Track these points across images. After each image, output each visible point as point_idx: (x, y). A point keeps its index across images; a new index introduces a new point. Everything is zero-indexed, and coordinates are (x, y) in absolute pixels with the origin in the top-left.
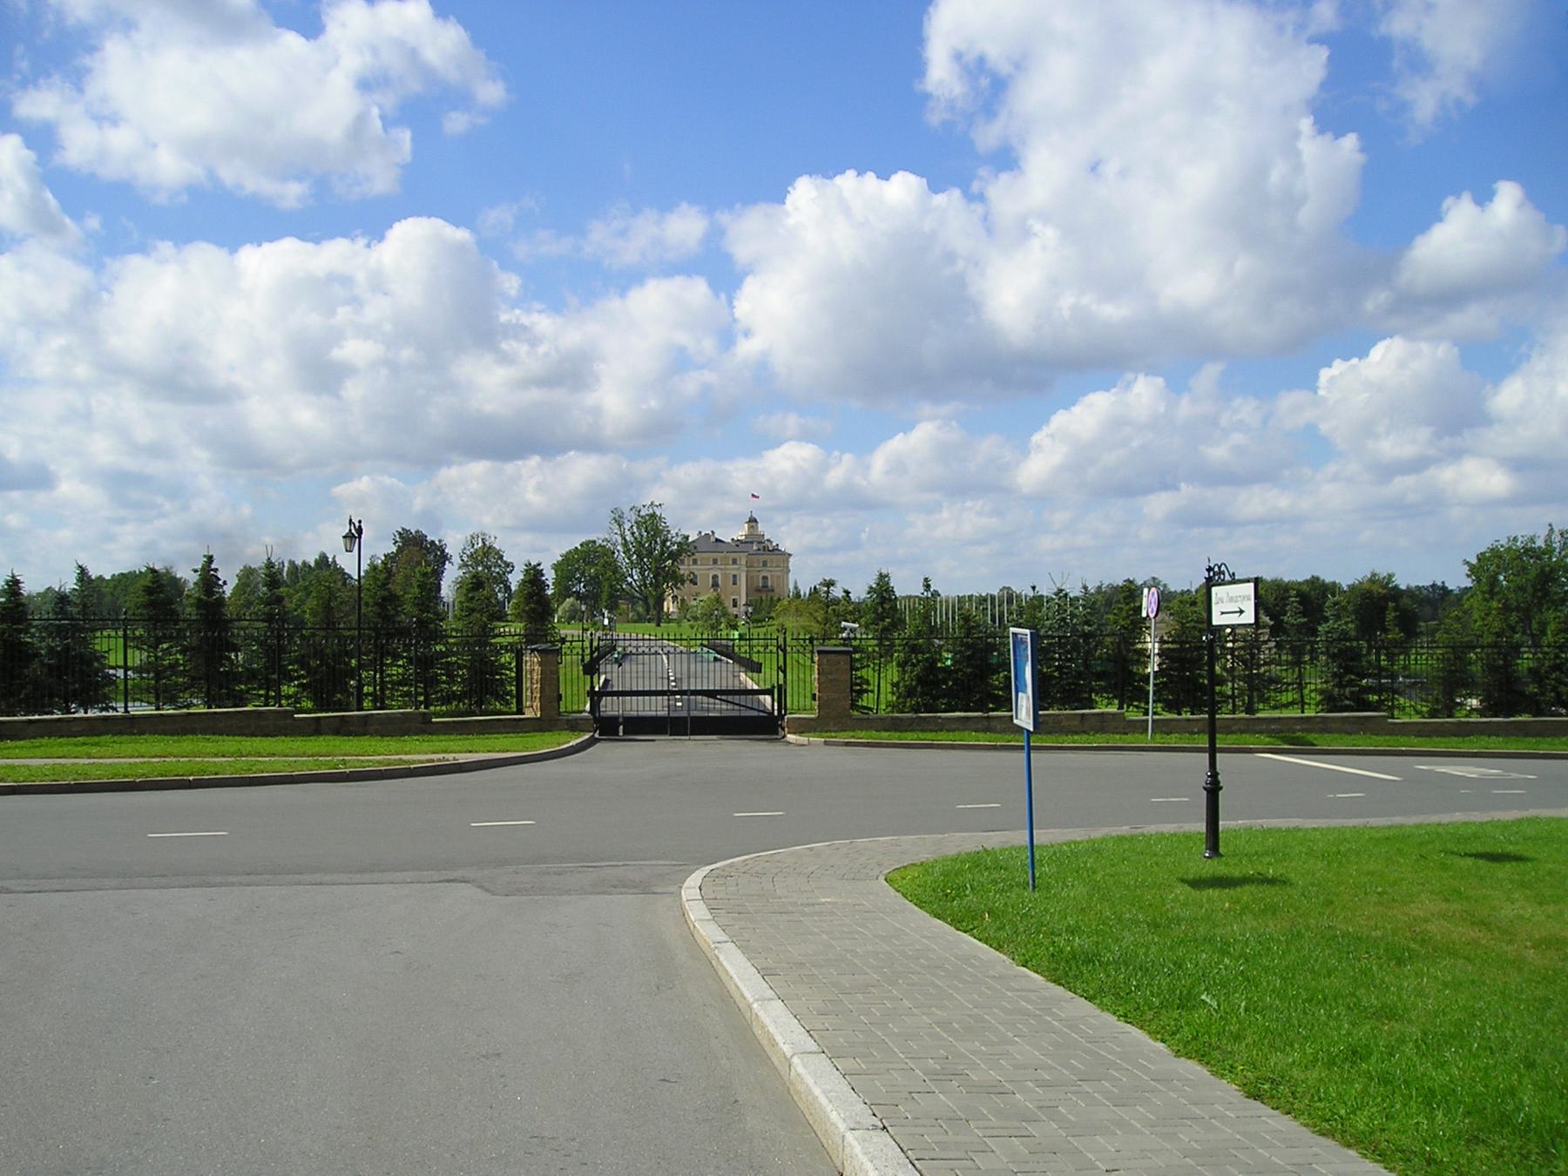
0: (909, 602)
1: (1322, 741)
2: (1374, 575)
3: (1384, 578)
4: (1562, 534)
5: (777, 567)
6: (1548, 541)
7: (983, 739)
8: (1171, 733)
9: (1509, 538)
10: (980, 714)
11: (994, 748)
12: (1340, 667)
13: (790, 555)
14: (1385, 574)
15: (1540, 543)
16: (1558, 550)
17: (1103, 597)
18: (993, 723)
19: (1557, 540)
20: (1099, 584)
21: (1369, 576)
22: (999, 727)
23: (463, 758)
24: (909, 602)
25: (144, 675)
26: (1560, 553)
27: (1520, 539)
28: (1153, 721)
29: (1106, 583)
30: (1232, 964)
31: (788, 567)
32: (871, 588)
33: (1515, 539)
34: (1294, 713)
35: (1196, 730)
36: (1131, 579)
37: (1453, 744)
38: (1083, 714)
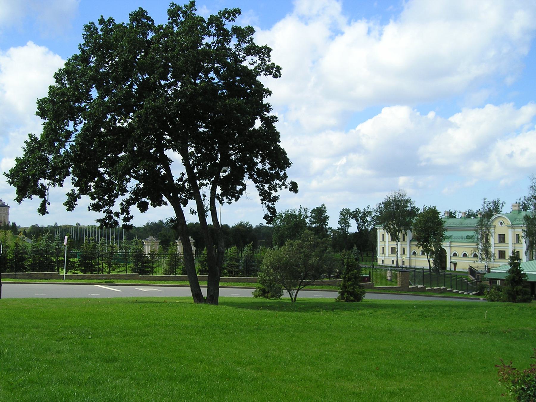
0: (60, 229)
1: (116, 282)
2: (241, 222)
3: (245, 224)
4: (305, 209)
5: (3, 212)
6: (300, 211)
7: (12, 280)
8: (72, 279)
9: (286, 210)
10: (13, 273)
11: (15, 283)
12: (136, 260)
13: (10, 207)
14: (245, 222)
15: (297, 213)
16: (303, 215)
17: (149, 227)
18: (17, 276)
19: (303, 211)
20: (148, 222)
21: (240, 223)
22: (19, 277)
23: (377, 292)
24: (60, 229)
25: (151, 126)
26: (304, 216)
27: (290, 210)
28: (65, 275)
29: (151, 221)
30: (511, 396)
31: (8, 212)
32: (258, 190)
33: (288, 211)
34: (124, 273)
35: (80, 278)
36: (161, 220)
37: (152, 283)
38: (45, 273)
